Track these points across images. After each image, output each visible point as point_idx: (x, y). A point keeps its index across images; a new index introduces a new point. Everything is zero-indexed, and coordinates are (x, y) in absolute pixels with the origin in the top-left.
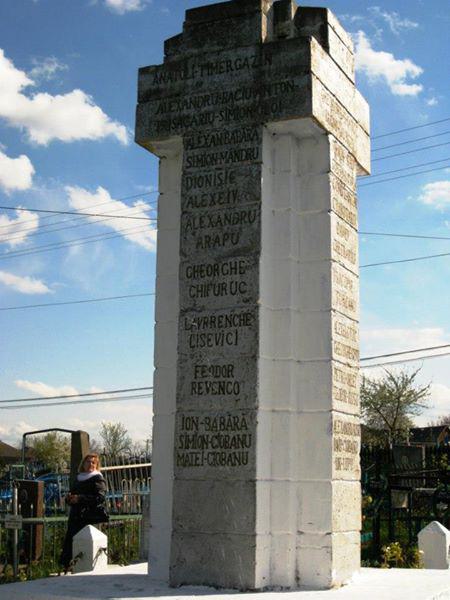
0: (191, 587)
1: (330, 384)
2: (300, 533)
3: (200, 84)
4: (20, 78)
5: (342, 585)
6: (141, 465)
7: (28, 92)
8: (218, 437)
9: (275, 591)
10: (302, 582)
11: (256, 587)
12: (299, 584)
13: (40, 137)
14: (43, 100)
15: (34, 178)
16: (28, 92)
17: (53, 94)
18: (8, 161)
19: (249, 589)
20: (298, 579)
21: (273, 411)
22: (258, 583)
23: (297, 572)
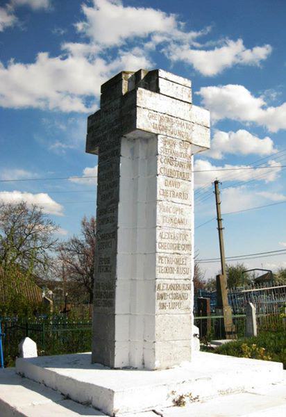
0: (97, 364)
1: (155, 265)
2: (145, 341)
3: (104, 121)
4: (259, 102)
5: (168, 368)
6: (261, 289)
7: (263, 108)
8: (105, 293)
9: (256, 358)
10: (145, 366)
11: (115, 367)
12: (144, 367)
13: (273, 129)
14: (271, 110)
15: (274, 147)
16: (263, 108)
17: (275, 107)
18: (261, 141)
19: (112, 368)
20: (143, 364)
21: (132, 279)
22: (117, 363)
23: (143, 360)
